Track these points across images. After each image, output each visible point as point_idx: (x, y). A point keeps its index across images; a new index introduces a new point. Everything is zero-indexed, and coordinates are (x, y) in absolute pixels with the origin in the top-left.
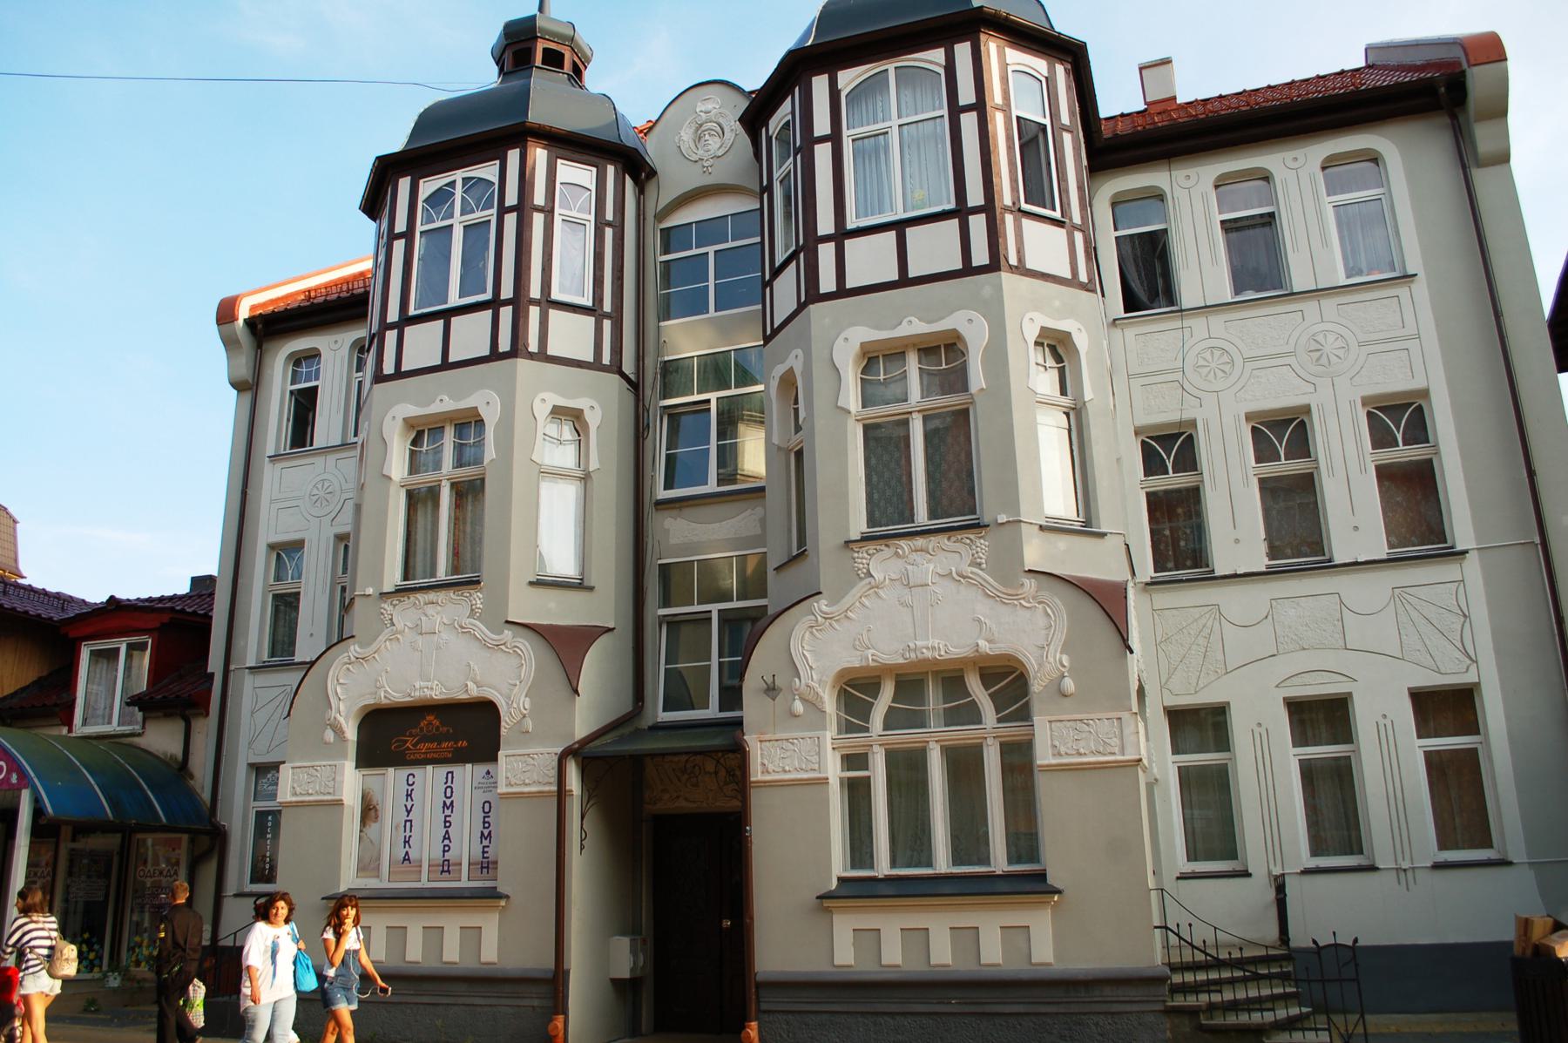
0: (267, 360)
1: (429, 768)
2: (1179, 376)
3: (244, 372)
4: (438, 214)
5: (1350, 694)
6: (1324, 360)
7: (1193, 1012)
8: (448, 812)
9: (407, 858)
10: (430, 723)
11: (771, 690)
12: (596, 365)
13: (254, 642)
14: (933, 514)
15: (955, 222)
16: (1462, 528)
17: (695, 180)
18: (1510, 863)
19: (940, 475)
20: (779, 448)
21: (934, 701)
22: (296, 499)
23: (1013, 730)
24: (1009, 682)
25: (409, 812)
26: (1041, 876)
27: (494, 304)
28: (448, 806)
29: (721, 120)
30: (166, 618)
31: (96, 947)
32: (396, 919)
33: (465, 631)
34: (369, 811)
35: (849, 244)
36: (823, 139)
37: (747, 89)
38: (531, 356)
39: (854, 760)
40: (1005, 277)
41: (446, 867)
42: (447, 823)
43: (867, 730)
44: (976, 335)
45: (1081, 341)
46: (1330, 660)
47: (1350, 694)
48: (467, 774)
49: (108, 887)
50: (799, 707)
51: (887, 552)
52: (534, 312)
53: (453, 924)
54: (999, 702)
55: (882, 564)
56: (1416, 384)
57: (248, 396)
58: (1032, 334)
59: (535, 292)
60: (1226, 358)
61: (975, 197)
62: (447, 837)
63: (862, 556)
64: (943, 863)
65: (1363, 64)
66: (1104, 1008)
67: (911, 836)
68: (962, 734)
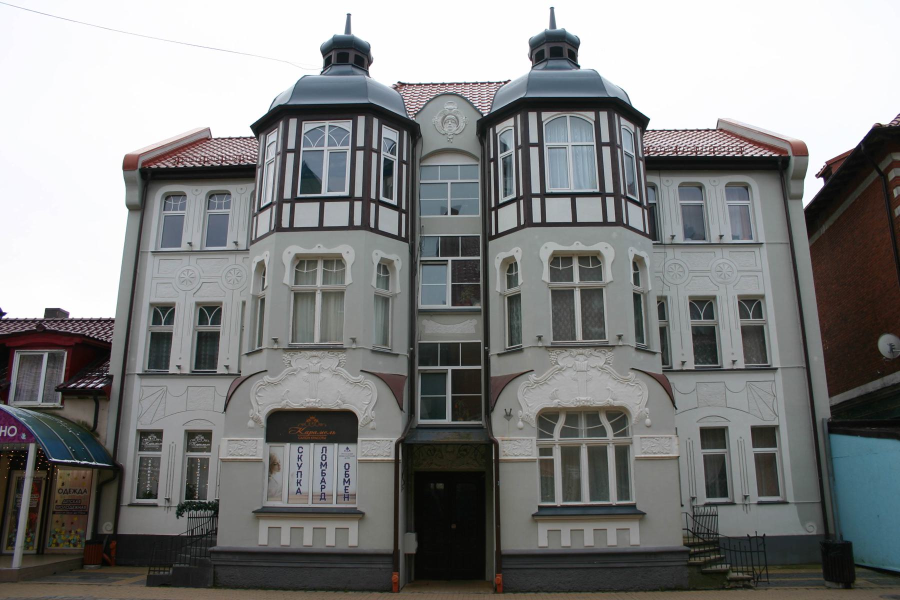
1: (312, 444)
2: (661, 275)
3: (136, 199)
4: (314, 142)
5: (727, 427)
6: (723, 276)
7: (698, 565)
8: (323, 468)
9: (299, 491)
10: (312, 421)
11: (508, 416)
12: (398, 237)
14: (586, 336)
16: (775, 359)
18: (788, 503)
20: (500, 294)
21: (583, 426)
22: (166, 281)
23: (622, 440)
25: (300, 468)
27: (351, 198)
28: (324, 465)
30: (77, 340)
31: (31, 535)
32: (297, 524)
33: (336, 374)
38: (372, 230)
39: (546, 451)
41: (323, 497)
42: (323, 474)
43: (552, 437)
45: (647, 262)
47: (727, 427)
48: (334, 450)
49: (39, 499)
51: (566, 354)
52: (373, 206)
53: (331, 527)
54: (615, 427)
55: (565, 359)
57: (138, 216)
59: (536, 189)
60: (681, 269)
61: (609, 189)
62: (323, 481)
63: (553, 354)
65: (715, 128)
66: (662, 564)
67: (572, 488)
68: (596, 440)
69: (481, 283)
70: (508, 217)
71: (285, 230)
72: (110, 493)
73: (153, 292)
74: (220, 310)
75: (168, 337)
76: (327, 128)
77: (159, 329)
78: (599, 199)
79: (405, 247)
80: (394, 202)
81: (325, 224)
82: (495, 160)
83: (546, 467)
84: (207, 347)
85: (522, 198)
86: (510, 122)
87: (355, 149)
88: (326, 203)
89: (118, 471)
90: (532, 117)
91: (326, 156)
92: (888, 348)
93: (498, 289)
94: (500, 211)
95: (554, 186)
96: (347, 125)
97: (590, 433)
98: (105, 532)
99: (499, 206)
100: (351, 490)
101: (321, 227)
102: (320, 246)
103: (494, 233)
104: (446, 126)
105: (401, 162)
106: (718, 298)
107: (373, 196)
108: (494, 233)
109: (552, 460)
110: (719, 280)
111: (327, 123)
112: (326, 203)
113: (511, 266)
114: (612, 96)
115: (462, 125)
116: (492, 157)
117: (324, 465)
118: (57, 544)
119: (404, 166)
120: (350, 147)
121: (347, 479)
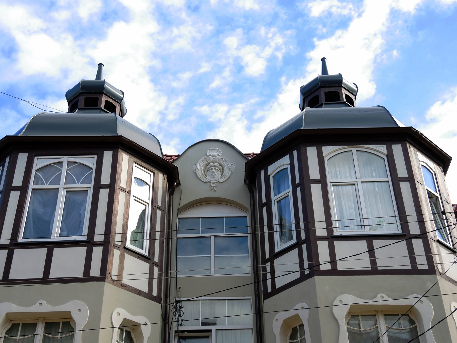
4: (47, 181)
12: (149, 295)
15: (83, 250)
17: (205, 193)
27: (89, 244)
29: (222, 162)
35: (17, 253)
36: (16, 189)
37: (244, 152)
38: (325, 273)
40: (108, 287)
44: (426, 311)
52: (116, 253)
58: (117, 322)
59: (321, 231)
61: (99, 237)
70: (287, 266)
76: (65, 165)
79: (157, 308)
80: (145, 252)
81: (53, 274)
82: (268, 204)
85: (304, 242)
87: (98, 186)
88: (56, 250)
90: (311, 152)
91: (62, 196)
95: (342, 227)
96: (90, 161)
99: (275, 255)
101: (46, 279)
102: (42, 304)
103: (269, 290)
108: (269, 290)
111: (65, 159)
112: (56, 250)
113: (294, 330)
115: (227, 173)
116: (264, 200)
119: (159, 213)
120: (92, 185)
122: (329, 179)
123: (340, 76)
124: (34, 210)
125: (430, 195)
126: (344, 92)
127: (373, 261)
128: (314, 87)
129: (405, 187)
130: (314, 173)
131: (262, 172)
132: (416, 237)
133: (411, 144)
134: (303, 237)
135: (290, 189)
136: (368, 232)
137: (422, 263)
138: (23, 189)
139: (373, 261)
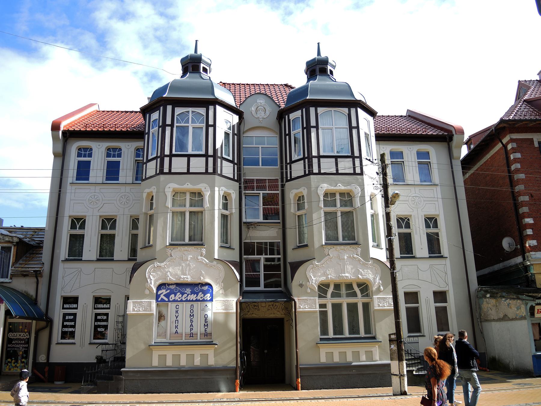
0: (68, 147)
3: (60, 150)
8: (192, 318)
9: (176, 332)
12: (233, 179)
13: (63, 251)
19: (346, 230)
21: (343, 291)
23: (366, 300)
24: (364, 287)
26: (374, 338)
27: (206, 156)
28: (192, 316)
34: (161, 317)
39: (322, 306)
41: (191, 335)
42: (191, 321)
43: (326, 297)
44: (357, 190)
46: (415, 282)
50: (309, 291)
52: (219, 160)
54: (362, 291)
55: (333, 252)
56: (437, 213)
57: (60, 160)
59: (314, 153)
61: (211, 152)
62: (191, 325)
63: (327, 249)
64: (347, 334)
68: (352, 300)
69: (280, 207)
70: (298, 169)
71: (166, 173)
72: (44, 335)
73: (71, 209)
74: (85, 221)
75: (112, 237)
77: (74, 232)
78: (204, 159)
80: (230, 158)
82: (289, 134)
83: (323, 314)
84: (107, 244)
86: (298, 114)
87: (208, 126)
89: (50, 322)
90: (312, 110)
92: (508, 245)
93: (292, 210)
94: (292, 165)
97: (348, 295)
98: (41, 361)
99: (292, 162)
100: (209, 331)
104: (258, 113)
105: (234, 134)
106: (413, 216)
107: (219, 155)
109: (326, 311)
110: (413, 206)
111: (190, 109)
114: (358, 99)
116: (287, 133)
117: (192, 316)
118: (10, 369)
120: (205, 125)
121: (206, 324)
122: (320, 126)
123: (327, 58)
124: (178, 137)
125: (366, 134)
126: (329, 68)
127: (337, 170)
128: (313, 64)
129: (354, 131)
130: (313, 123)
131: (287, 116)
132: (357, 157)
133: (360, 108)
134: (306, 156)
135: (301, 129)
136: (336, 154)
137: (358, 170)
138: (172, 126)
139: (337, 170)
